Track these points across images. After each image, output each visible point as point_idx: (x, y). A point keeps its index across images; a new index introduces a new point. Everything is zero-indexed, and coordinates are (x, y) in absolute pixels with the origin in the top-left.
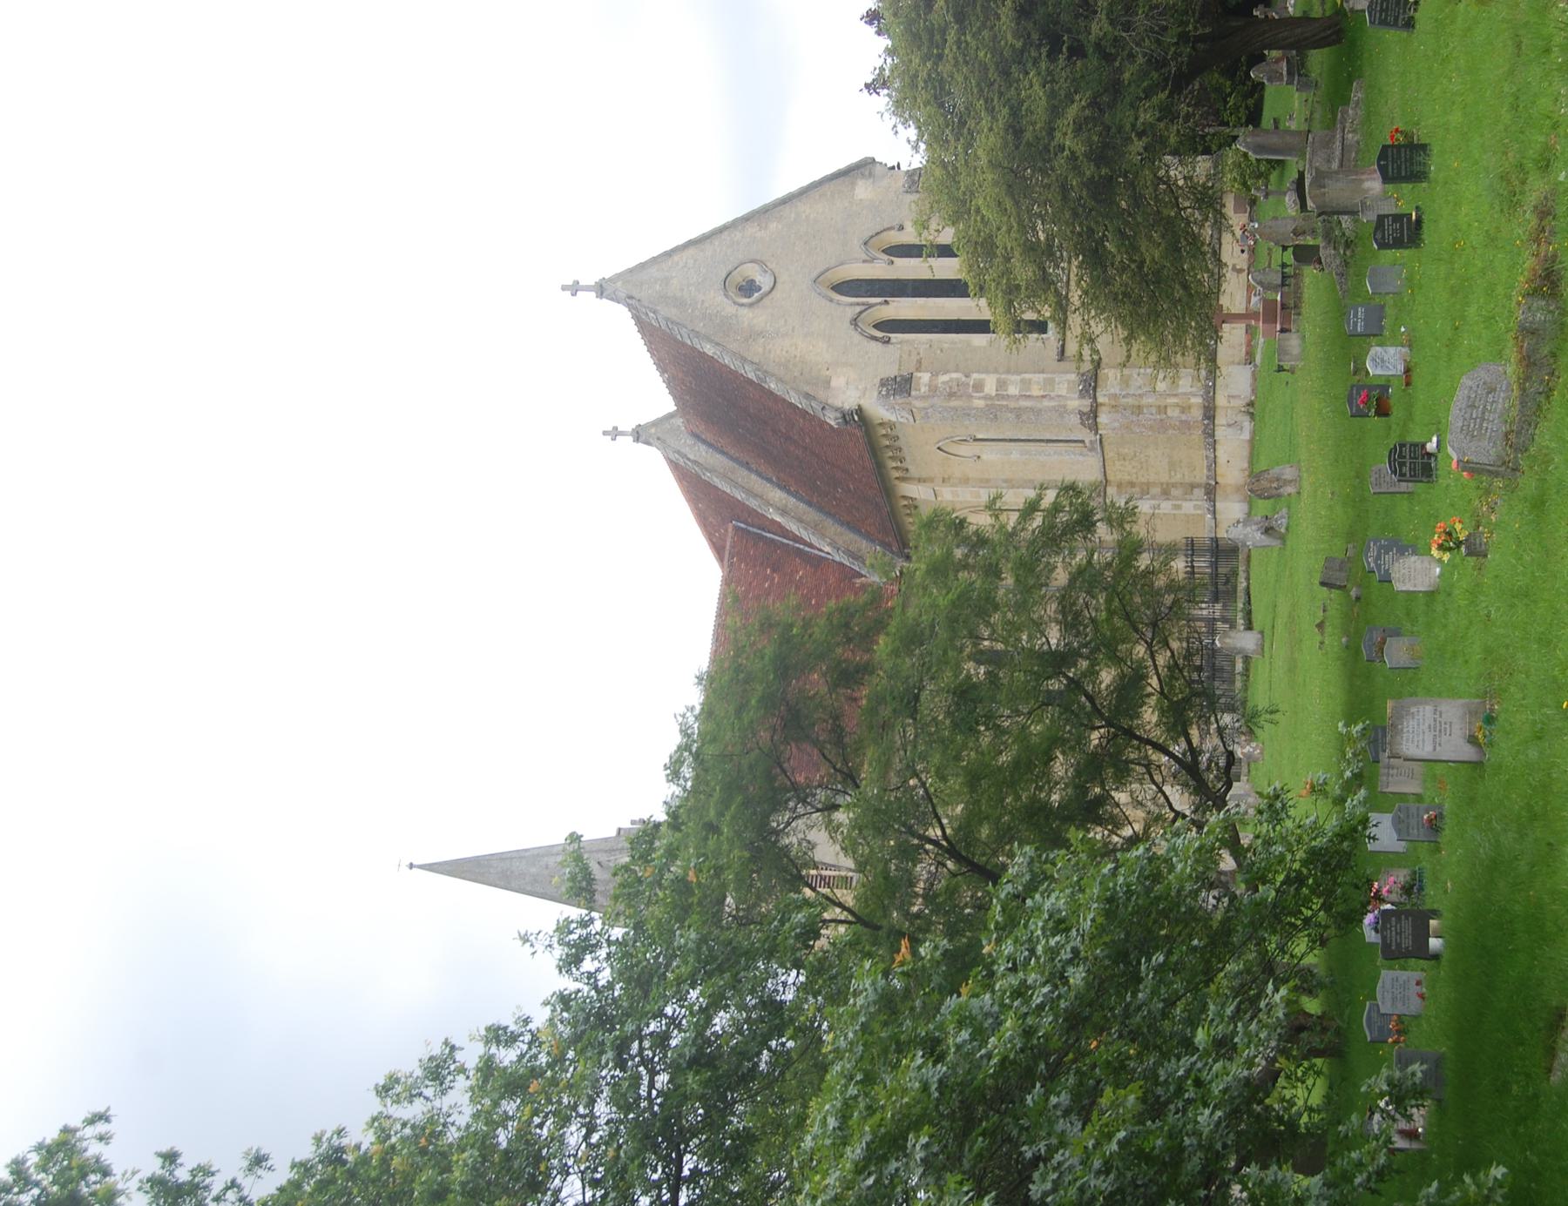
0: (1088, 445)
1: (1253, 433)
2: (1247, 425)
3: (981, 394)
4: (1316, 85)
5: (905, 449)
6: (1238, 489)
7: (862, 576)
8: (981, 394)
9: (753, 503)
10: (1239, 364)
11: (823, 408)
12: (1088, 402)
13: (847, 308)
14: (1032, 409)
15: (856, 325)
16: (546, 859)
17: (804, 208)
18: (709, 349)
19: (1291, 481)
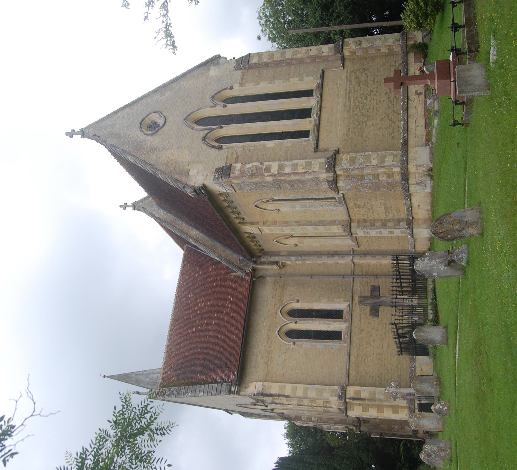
0: (338, 200)
1: (433, 188)
2: (429, 183)
3: (269, 174)
6: (425, 221)
7: (234, 272)
8: (269, 174)
10: (421, 146)
11: (184, 187)
14: (299, 181)
16: (152, 375)
19: (472, 223)
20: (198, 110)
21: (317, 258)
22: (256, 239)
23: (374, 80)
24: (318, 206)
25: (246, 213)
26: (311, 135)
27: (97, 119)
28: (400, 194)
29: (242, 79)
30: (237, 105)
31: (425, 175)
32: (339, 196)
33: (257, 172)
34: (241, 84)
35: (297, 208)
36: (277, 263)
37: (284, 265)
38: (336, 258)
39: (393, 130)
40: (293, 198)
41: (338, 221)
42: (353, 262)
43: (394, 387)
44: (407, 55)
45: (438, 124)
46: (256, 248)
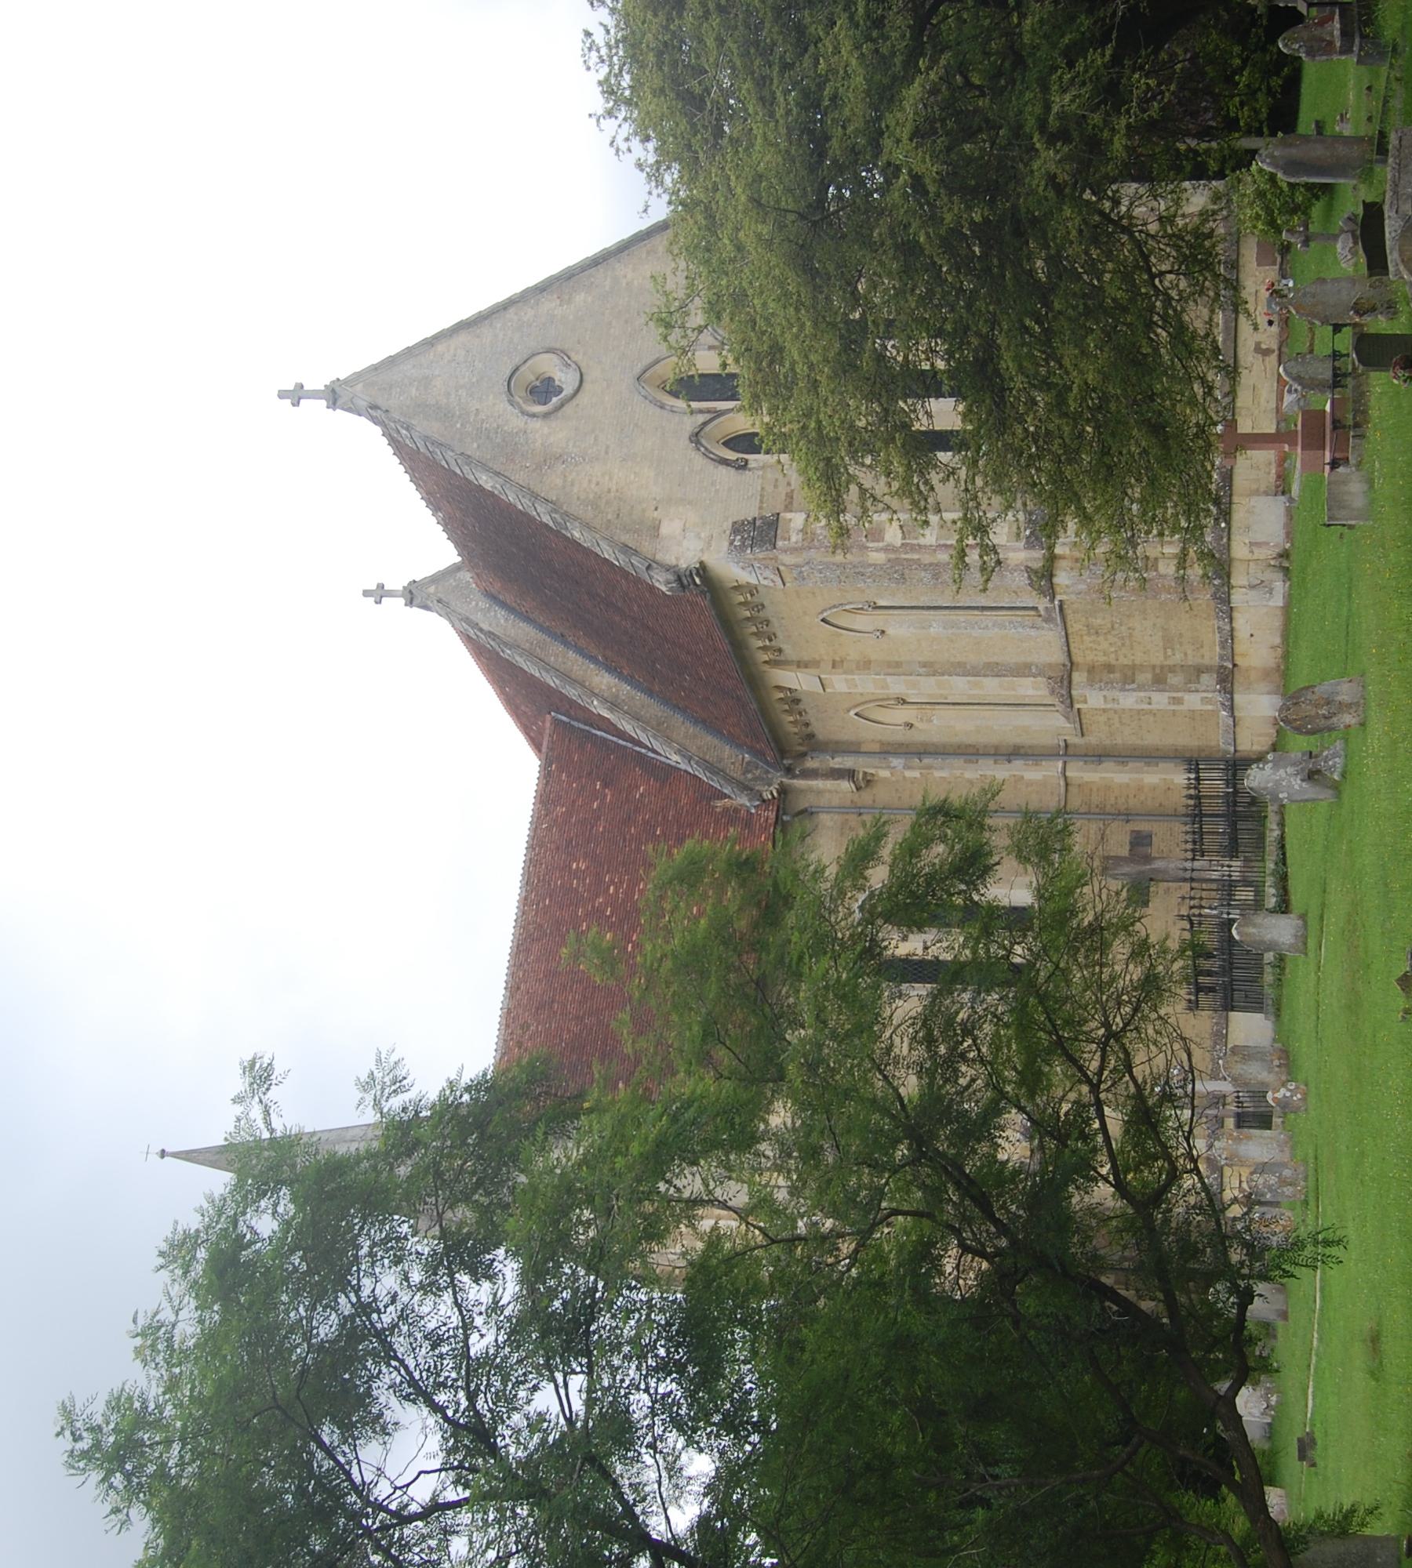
0: (1042, 613)
2: (1279, 586)
3: (881, 544)
4: (1394, 49)
5: (774, 620)
6: (1266, 674)
7: (726, 796)
8: (881, 544)
9: (572, 692)
10: (1266, 493)
11: (649, 567)
13: (685, 418)
15: (698, 443)
18: (486, 481)
19: (1349, 706)
21: (965, 762)
22: (801, 706)
24: (990, 625)
25: (789, 637)
27: (376, 359)
28: (1204, 606)
31: (1270, 565)
35: (932, 630)
36: (850, 774)
37: (869, 781)
38: (1018, 763)
42: (1066, 778)
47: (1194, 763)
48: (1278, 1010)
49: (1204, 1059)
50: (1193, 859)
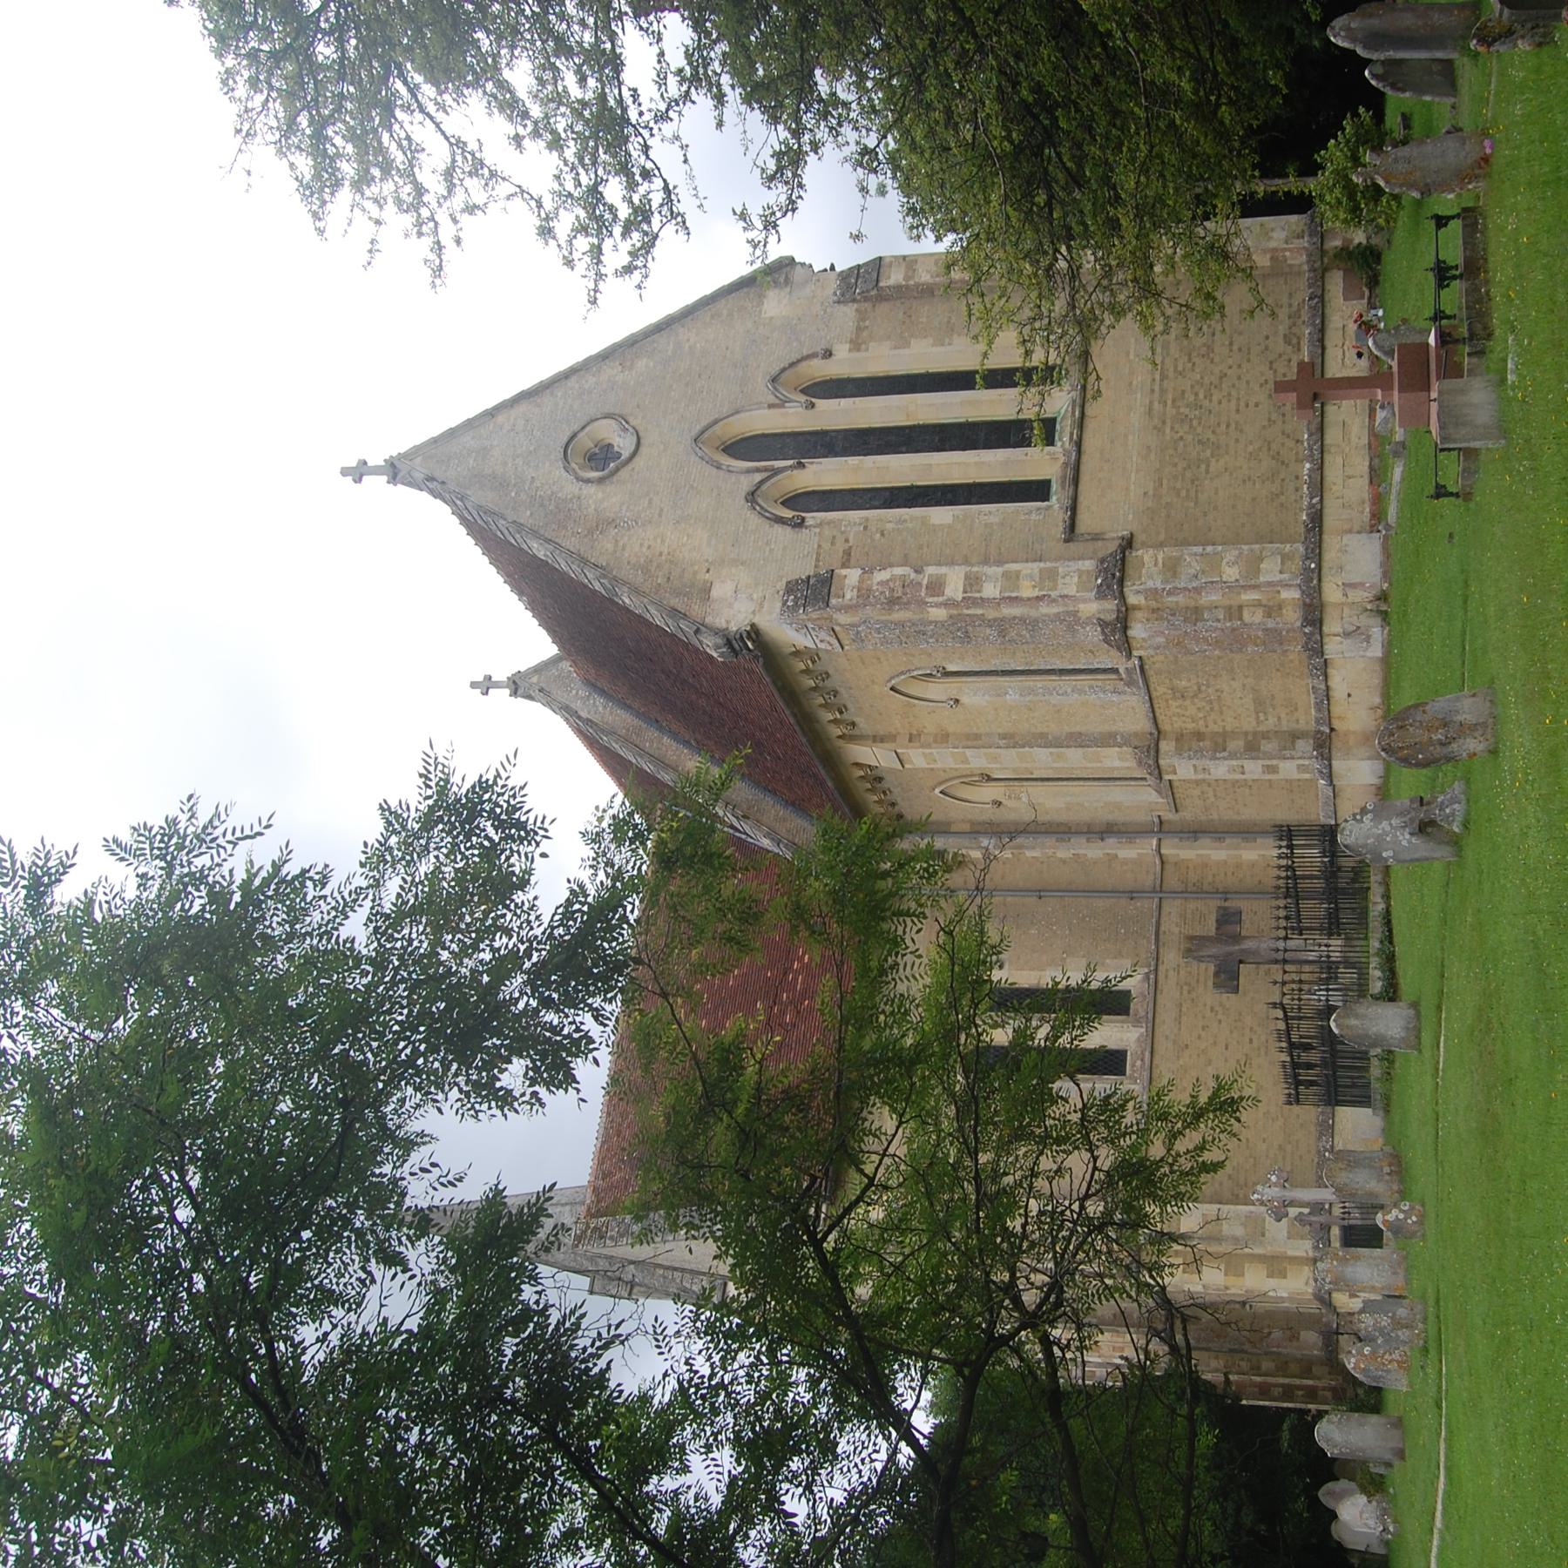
1: (1388, 646)
2: (1377, 633)
3: (941, 599)
5: (842, 690)
6: (1366, 738)
8: (941, 599)
10: (1359, 532)
11: (697, 631)
12: (1111, 605)
14: (1022, 620)
17: (687, 335)
19: (1474, 727)
20: (732, 415)
22: (885, 785)
23: (1231, 344)
24: (1069, 690)
26: (1056, 493)
27: (436, 432)
28: (1297, 662)
29: (859, 329)
30: (845, 403)
31: (1367, 610)
32: (1130, 665)
33: (905, 594)
34: (856, 345)
38: (1111, 841)
39: (1282, 487)
40: (1000, 668)
41: (1122, 736)
42: (1161, 856)
43: (1275, 1185)
44: (1323, 277)
45: (1403, 479)
46: (882, 810)
47: (1287, 834)
48: (1388, 1105)
49: (1309, 1152)
50: (1286, 938)
